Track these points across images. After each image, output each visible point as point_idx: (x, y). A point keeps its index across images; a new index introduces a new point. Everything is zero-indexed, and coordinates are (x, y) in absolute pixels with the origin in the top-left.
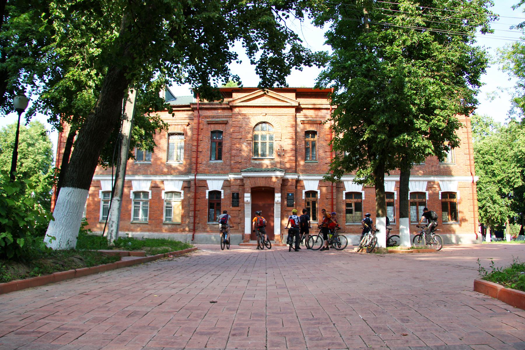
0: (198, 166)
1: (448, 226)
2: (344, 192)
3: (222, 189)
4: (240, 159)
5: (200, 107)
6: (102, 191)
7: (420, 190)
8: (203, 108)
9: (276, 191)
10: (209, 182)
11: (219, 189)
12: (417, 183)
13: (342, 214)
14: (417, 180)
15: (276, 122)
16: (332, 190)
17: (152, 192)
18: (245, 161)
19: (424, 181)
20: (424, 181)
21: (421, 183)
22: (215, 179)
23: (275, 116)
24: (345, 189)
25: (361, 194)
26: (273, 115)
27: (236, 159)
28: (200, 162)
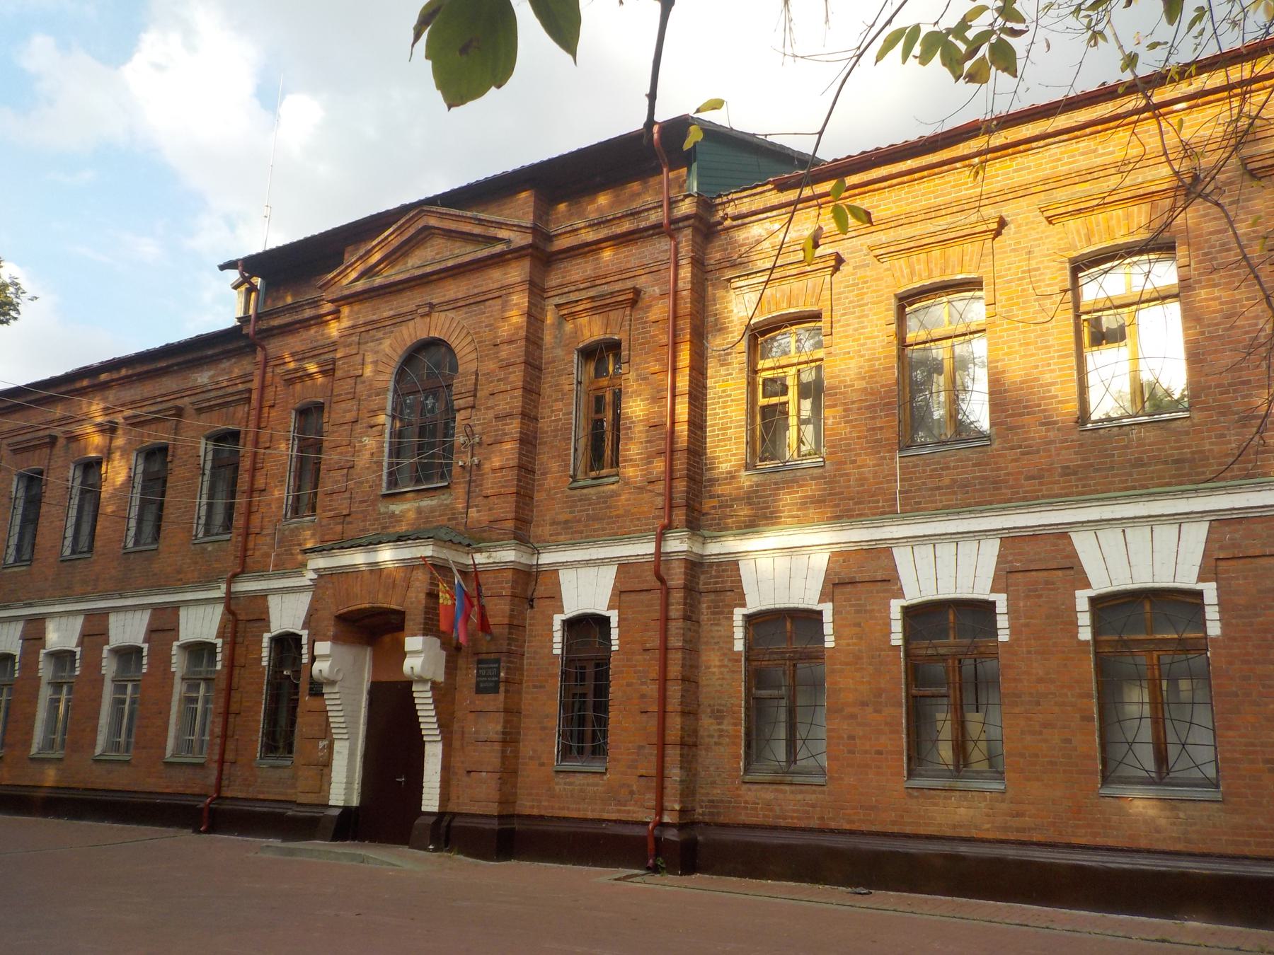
0: (251, 545)
1: (1122, 802)
2: (738, 614)
3: (823, 598)
4: (346, 503)
6: (1092, 593)
7: (964, 592)
8: (274, 328)
9: (409, 624)
10: (1083, 544)
11: (982, 591)
12: (1138, 536)
13: (726, 726)
14: (1134, 519)
15: (465, 331)
16: (666, 605)
17: (835, 612)
18: (363, 507)
19: (1178, 519)
20: (1178, 519)
21: (968, 548)
22: (588, 563)
23: (465, 309)
24: (742, 596)
25: (814, 617)
26: (454, 305)
27: (335, 505)
28: (257, 530)
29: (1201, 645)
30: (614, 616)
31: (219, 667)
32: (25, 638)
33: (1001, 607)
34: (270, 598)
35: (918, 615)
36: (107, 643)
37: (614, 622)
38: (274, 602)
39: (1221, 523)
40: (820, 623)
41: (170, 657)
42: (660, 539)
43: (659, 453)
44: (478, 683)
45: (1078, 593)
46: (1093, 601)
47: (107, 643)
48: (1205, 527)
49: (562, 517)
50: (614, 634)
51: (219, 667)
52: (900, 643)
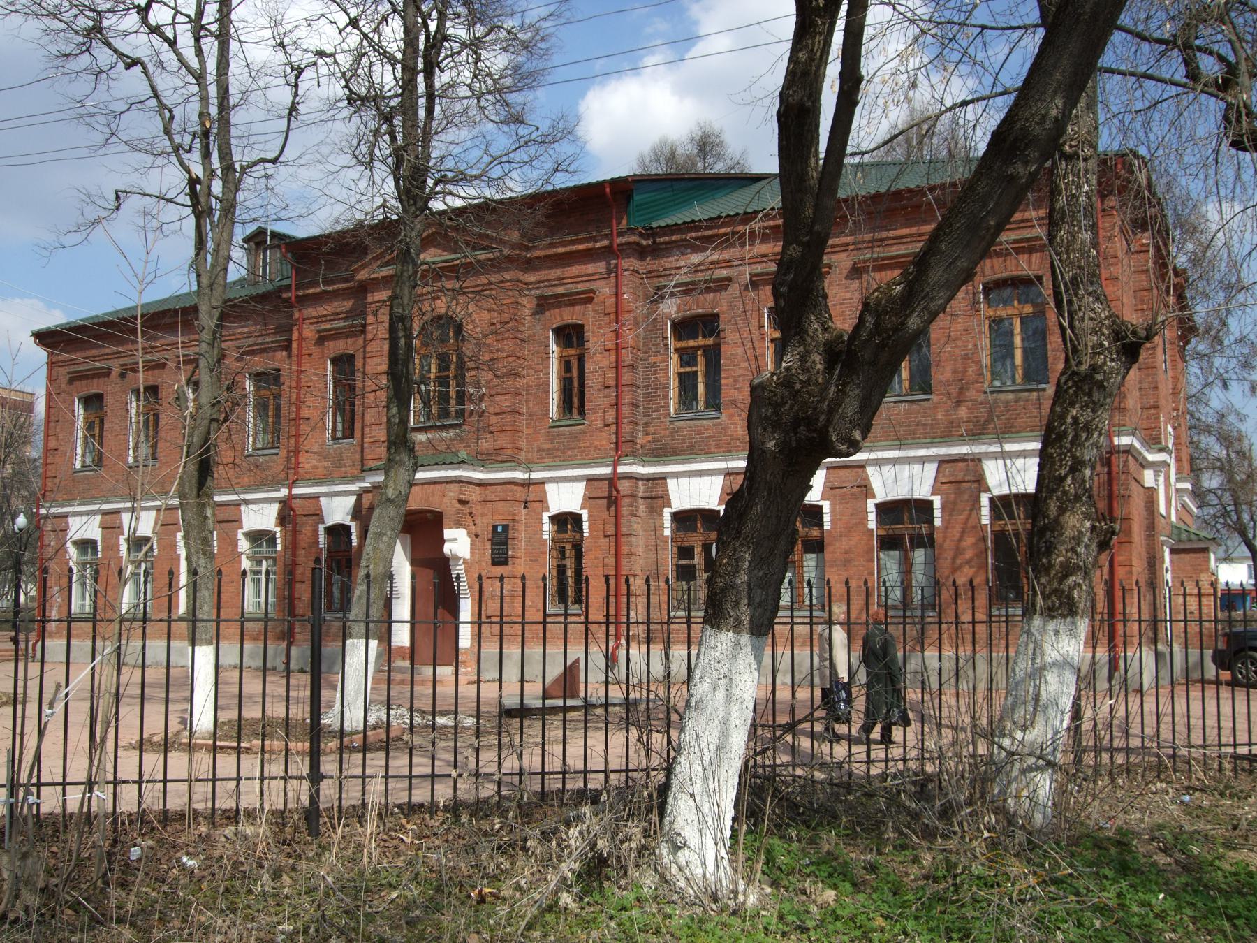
5: (300, 293)
6: (877, 501)
9: (446, 521)
17: (590, 516)
20: (923, 460)
24: (669, 500)
29: (212, 553)
30: (585, 515)
31: (279, 548)
32: (104, 527)
33: (826, 509)
34: (669, 481)
35: (885, 509)
36: (241, 528)
37: (585, 517)
38: (671, 483)
39: (943, 462)
40: (932, 510)
41: (118, 545)
42: (615, 465)
43: (612, 405)
44: (493, 559)
45: (869, 501)
46: (877, 506)
47: (241, 528)
48: (935, 466)
49: (545, 446)
50: (585, 525)
51: (279, 548)
52: (987, 522)
